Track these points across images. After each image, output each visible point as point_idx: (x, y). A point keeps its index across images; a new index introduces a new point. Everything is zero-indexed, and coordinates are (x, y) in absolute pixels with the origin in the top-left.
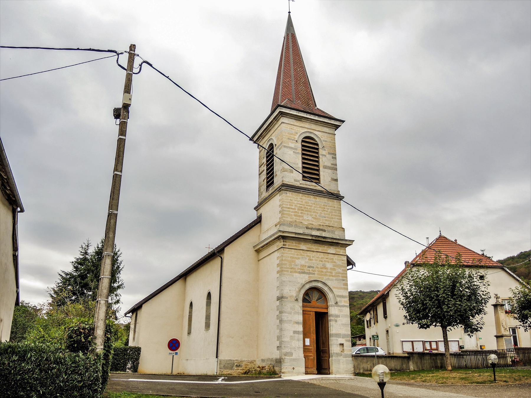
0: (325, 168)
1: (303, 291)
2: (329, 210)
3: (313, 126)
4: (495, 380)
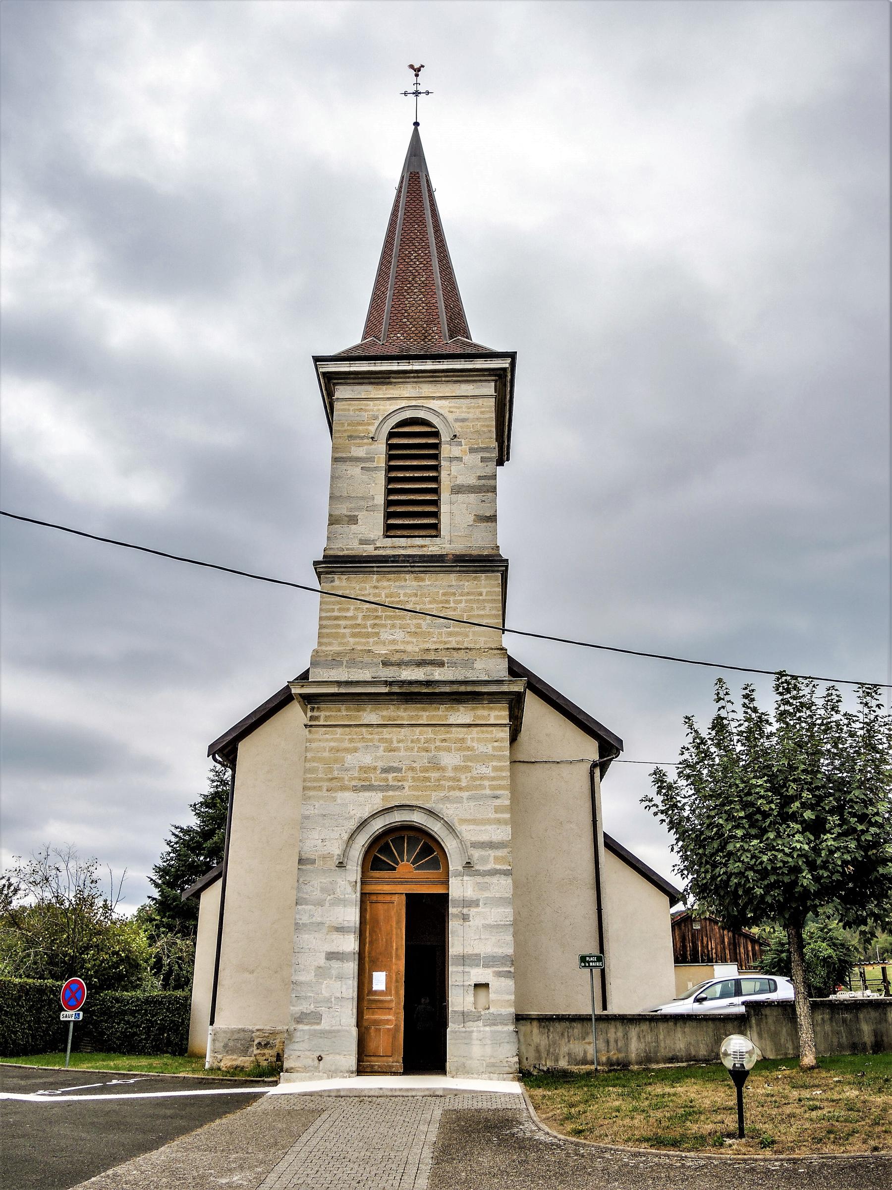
0: (458, 493)
1: (363, 840)
2: (463, 605)
3: (427, 389)
4: (741, 1129)
